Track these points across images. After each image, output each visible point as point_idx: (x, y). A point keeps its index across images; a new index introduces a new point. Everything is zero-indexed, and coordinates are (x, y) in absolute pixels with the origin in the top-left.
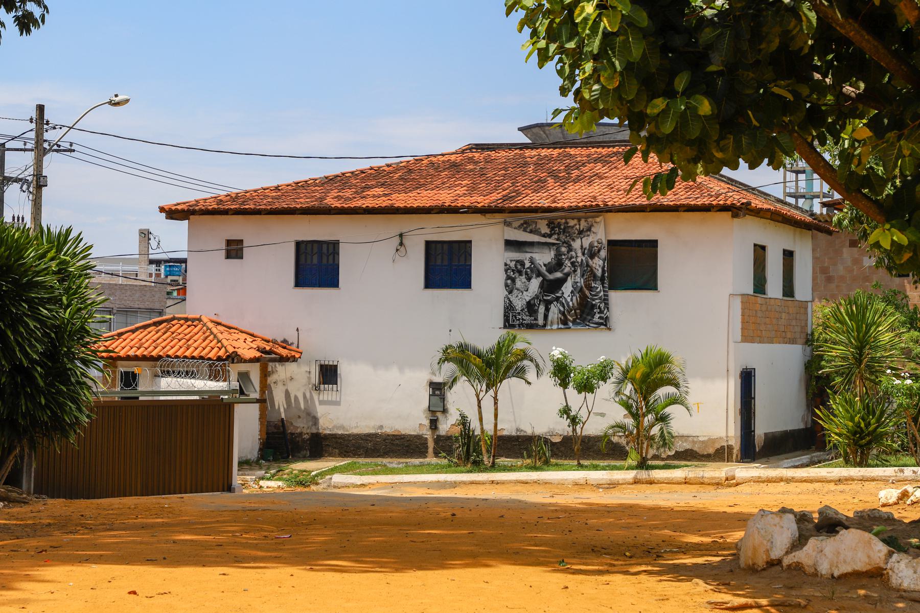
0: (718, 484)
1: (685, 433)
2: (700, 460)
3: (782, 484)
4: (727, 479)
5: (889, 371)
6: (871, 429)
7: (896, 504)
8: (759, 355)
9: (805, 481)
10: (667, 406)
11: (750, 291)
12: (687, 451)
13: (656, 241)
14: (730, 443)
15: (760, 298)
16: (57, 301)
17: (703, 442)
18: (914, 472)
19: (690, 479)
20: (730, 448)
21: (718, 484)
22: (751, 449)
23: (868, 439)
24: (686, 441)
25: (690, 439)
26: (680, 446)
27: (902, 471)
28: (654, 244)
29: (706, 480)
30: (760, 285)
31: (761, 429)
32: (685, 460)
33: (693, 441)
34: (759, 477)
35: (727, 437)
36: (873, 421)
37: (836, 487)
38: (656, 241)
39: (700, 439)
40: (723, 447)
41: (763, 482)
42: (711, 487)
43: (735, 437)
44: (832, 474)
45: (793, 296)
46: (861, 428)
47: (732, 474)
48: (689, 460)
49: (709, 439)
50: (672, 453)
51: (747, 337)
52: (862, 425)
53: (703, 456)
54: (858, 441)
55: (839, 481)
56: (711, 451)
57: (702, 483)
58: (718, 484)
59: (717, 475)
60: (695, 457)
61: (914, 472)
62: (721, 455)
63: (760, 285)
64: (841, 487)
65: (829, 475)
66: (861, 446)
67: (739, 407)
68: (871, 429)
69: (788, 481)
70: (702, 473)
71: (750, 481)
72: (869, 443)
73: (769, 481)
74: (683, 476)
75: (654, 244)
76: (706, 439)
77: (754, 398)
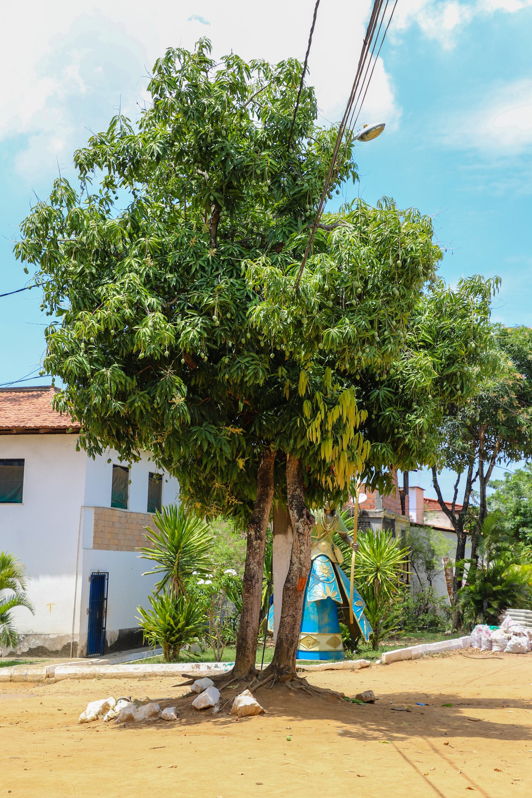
0: (39, 682)
1: (38, 631)
2: (49, 656)
3: (94, 680)
4: (48, 676)
5: (195, 573)
6: (179, 626)
7: (94, 720)
8: (108, 561)
9: (115, 677)
10: (11, 606)
11: (108, 503)
12: (39, 648)
13: (23, 460)
14: (75, 640)
15: (119, 511)
16: (254, 559)
17: (52, 639)
18: (209, 668)
19: (15, 677)
20: (75, 644)
21: (39, 681)
22: (97, 644)
23: (177, 636)
24: (38, 639)
25: (42, 637)
26: (35, 643)
27: (198, 667)
28: (21, 462)
29: (29, 678)
30: (120, 499)
31: (113, 626)
32: (37, 656)
33: (45, 639)
34: (75, 674)
35: (73, 634)
36: (182, 619)
37: (138, 684)
38: (23, 460)
39: (51, 637)
40: (69, 644)
41: (79, 678)
42: (33, 684)
43: (81, 635)
44: (139, 671)
45: (126, 508)
46: (171, 626)
47: (51, 671)
48: (40, 656)
49: (58, 637)
50: (26, 650)
51: (100, 543)
52: (172, 623)
53: (52, 652)
54: (169, 637)
55: (144, 677)
56: (59, 647)
57: (25, 681)
58: (39, 682)
59: (39, 673)
60: (45, 653)
61: (209, 668)
62: (67, 651)
63: (120, 499)
64: (143, 683)
65: (136, 671)
66: (172, 642)
67: (87, 606)
68: (179, 626)
69: (99, 677)
70: (25, 671)
71: (67, 678)
72: (178, 640)
73: (84, 677)
74: (9, 674)
75: (21, 462)
76: (55, 636)
77: (106, 599)
